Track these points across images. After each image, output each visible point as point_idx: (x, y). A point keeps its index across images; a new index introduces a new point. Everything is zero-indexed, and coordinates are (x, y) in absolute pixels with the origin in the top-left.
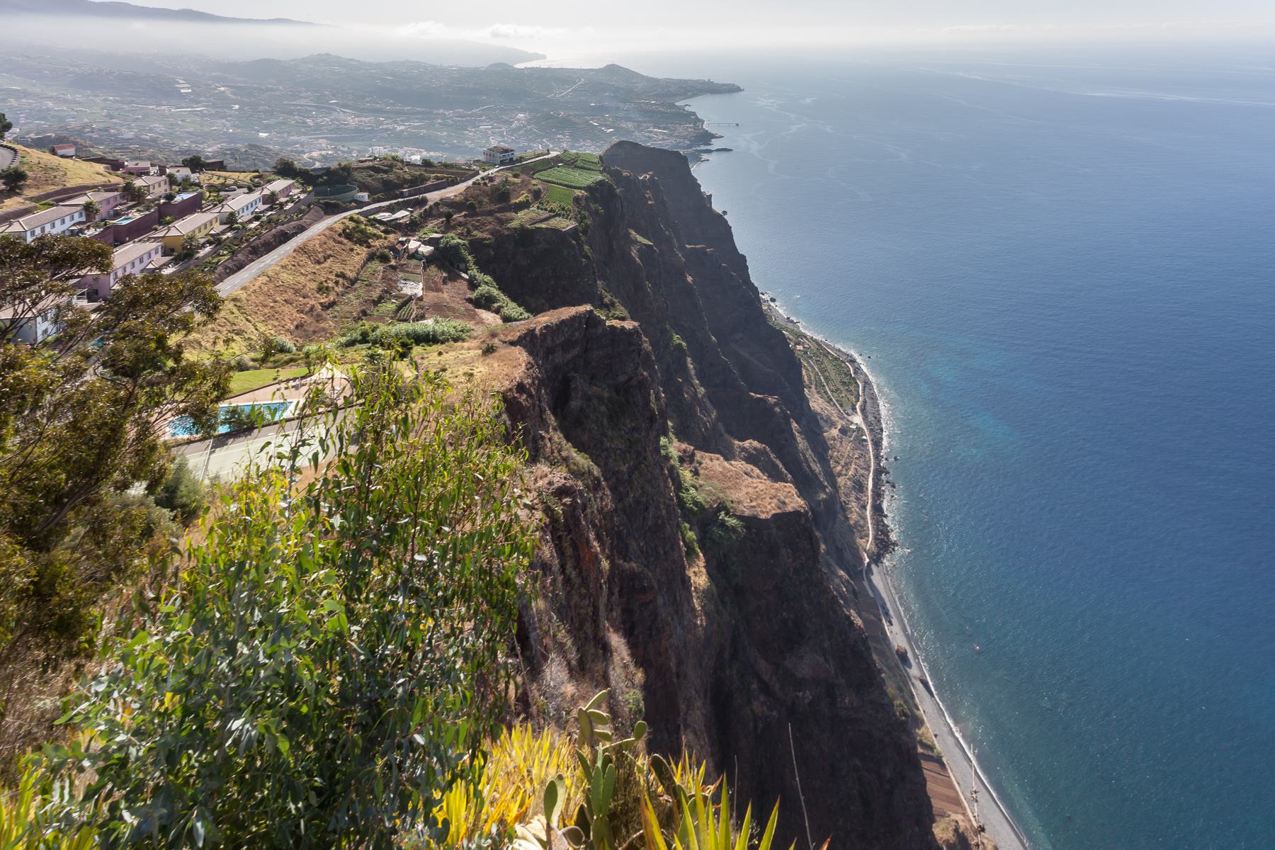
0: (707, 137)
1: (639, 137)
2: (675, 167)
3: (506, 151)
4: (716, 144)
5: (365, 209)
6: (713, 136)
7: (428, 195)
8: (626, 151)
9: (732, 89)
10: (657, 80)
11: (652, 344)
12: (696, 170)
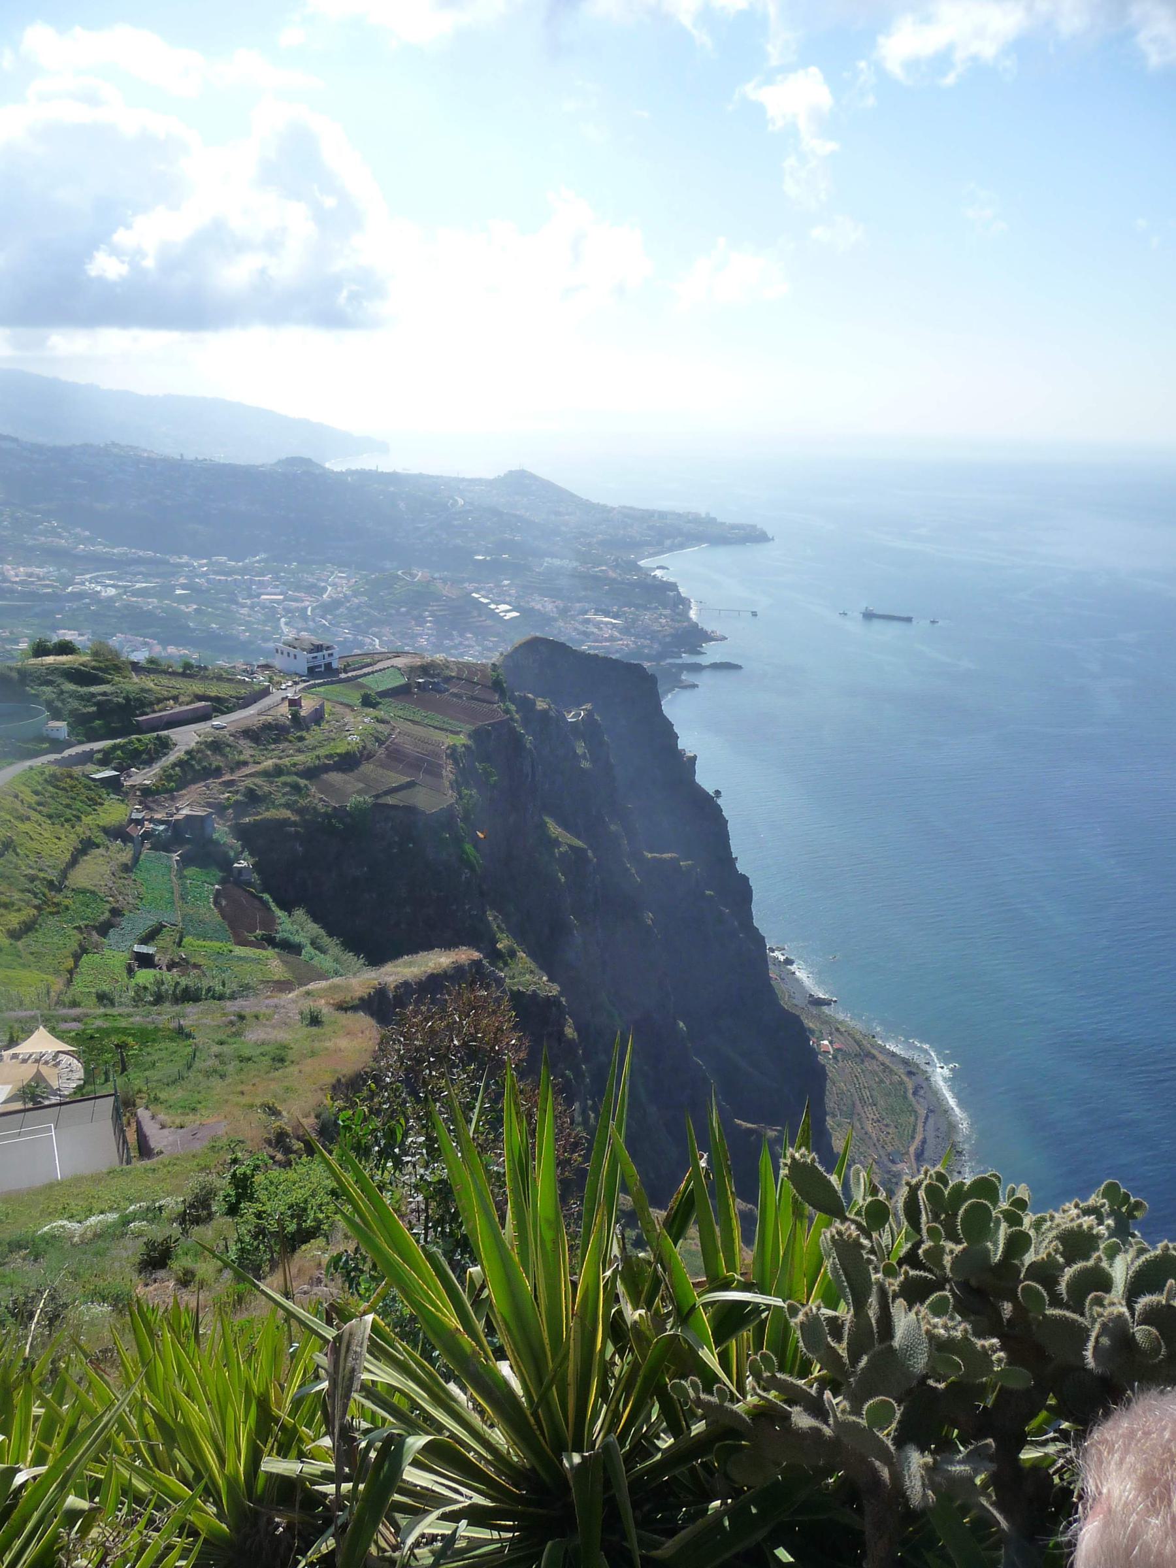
0: (695, 638)
1: (564, 631)
2: (632, 691)
3: (319, 648)
4: (712, 653)
5: (66, 753)
6: (707, 637)
7: (175, 734)
8: (545, 656)
9: (752, 536)
10: (604, 509)
11: (577, 1029)
12: (676, 708)
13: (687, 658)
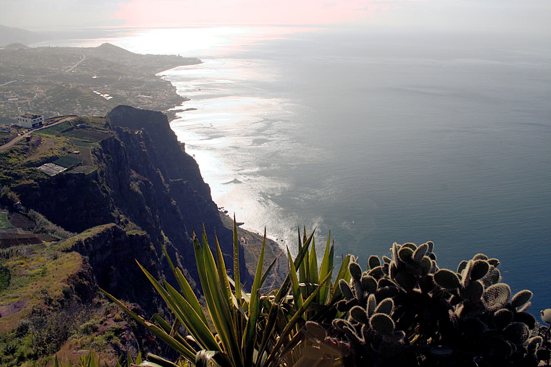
13: (177, 108)
